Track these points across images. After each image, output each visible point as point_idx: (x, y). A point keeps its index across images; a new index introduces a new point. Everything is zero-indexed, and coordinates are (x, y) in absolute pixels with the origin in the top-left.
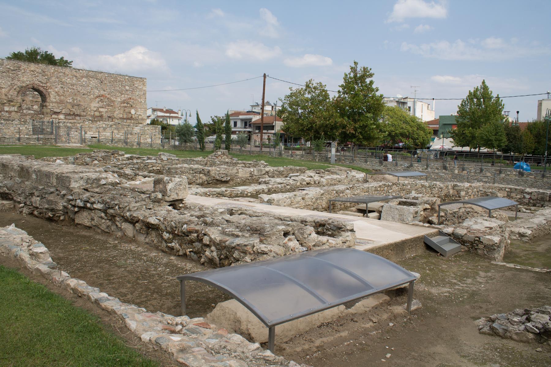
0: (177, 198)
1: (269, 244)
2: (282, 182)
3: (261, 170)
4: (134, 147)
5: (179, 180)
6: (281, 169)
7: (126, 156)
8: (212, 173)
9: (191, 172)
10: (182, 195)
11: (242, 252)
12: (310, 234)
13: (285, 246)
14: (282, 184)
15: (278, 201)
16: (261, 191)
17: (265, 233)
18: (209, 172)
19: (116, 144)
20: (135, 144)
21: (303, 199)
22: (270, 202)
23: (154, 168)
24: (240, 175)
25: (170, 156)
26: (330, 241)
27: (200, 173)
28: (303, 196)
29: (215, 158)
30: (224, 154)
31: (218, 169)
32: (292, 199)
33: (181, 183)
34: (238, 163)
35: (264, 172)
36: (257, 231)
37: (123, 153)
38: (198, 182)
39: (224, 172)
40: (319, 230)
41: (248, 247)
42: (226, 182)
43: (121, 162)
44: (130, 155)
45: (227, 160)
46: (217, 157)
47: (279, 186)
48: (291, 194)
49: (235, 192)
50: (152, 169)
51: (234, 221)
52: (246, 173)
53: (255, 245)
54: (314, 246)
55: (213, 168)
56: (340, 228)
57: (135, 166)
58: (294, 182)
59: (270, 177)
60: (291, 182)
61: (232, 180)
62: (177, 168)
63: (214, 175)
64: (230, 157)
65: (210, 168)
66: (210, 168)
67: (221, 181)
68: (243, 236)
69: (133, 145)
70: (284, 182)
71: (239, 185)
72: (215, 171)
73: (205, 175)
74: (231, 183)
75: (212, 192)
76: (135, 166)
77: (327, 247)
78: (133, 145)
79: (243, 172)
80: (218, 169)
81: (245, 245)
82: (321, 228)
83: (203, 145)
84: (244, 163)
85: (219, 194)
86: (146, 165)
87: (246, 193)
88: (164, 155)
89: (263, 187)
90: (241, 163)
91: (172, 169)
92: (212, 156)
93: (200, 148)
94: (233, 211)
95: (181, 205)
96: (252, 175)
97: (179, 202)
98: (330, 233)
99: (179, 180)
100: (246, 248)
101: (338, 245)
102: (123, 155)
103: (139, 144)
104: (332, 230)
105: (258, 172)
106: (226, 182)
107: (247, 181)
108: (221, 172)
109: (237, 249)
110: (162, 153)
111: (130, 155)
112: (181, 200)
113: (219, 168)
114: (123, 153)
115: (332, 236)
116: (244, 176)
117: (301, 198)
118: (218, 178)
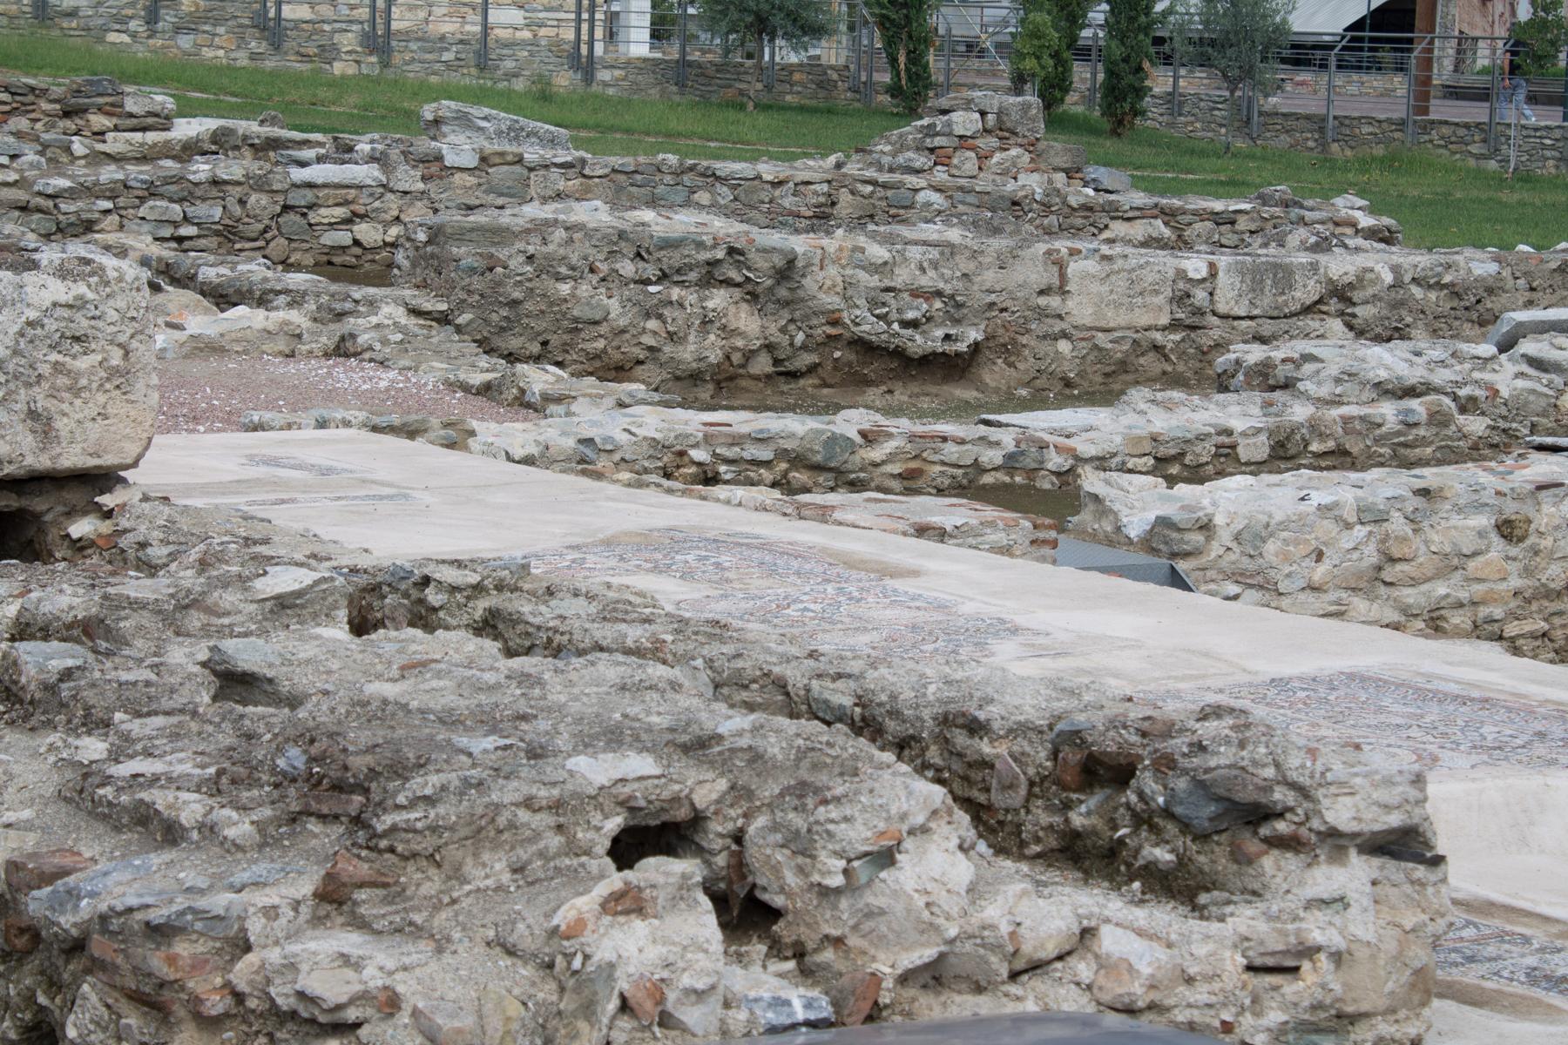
0: (43, 462)
1: (408, 931)
2: (1413, 374)
3: (1283, 276)
4: (338, 68)
5: (59, 291)
6: (1479, 265)
7: (187, 129)
8: (821, 288)
9: (628, 268)
10: (95, 430)
11: (137, 998)
12: (885, 858)
13: (557, 960)
14: (1411, 392)
15: (1252, 537)
16: (1205, 451)
17: (388, 820)
18: (787, 271)
19: (185, 41)
20: (348, 41)
21: (1508, 530)
22: (1168, 558)
23: (367, 232)
24: (1080, 309)
25: (515, 134)
26: (1111, 941)
27: (710, 277)
28: (1510, 509)
29: (921, 161)
30: (1003, 131)
31: (878, 252)
32: (1397, 524)
33: (82, 324)
34: (1114, 212)
35: (1307, 291)
36: (340, 796)
37: (163, 100)
38: (687, 353)
39: (927, 281)
40: (1078, 820)
41: (182, 948)
42: (951, 366)
43: (81, 171)
44: (212, 124)
45: (1032, 183)
46: (940, 157)
47: (1388, 411)
48: (1384, 484)
49: (951, 451)
50: (342, 237)
51: (304, 680)
52: (1137, 290)
53: (255, 926)
54: (934, 976)
55: (837, 241)
56: (1257, 815)
57: (200, 210)
58: (1539, 383)
59: (1359, 332)
60: (1507, 378)
61: (1001, 346)
62: (500, 235)
63: (831, 301)
64: (1059, 149)
65: (800, 244)
66: (800, 244)
67: (899, 354)
68: (209, 830)
69: (329, 53)
70: (1441, 377)
71: (1070, 391)
72: (842, 267)
73: (753, 297)
74: (994, 374)
75: (737, 440)
76: (200, 210)
77: (1071, 1001)
78: (329, 53)
79: (1110, 283)
80: (878, 252)
81: (160, 932)
82: (1093, 801)
83: (915, 58)
84: (1168, 215)
85: (798, 460)
86: (295, 205)
87: (1055, 461)
88: (464, 121)
89: (1239, 414)
90: (1141, 213)
91: (461, 235)
92: (901, 147)
93: (894, 90)
94: (433, 597)
95: (81, 528)
96: (1190, 313)
97: (73, 496)
98: (1163, 855)
99: (59, 291)
100: (157, 962)
101: (1200, 994)
102: (163, 121)
103: (379, 42)
104: (1185, 827)
105: (1257, 287)
106: (951, 366)
107: (1149, 361)
108: (902, 277)
109: (97, 966)
110: (448, 106)
111: (212, 124)
112: (101, 479)
113: (889, 240)
114: (163, 100)
115: (1180, 887)
116: (1114, 318)
117: (1484, 521)
118: (870, 327)
